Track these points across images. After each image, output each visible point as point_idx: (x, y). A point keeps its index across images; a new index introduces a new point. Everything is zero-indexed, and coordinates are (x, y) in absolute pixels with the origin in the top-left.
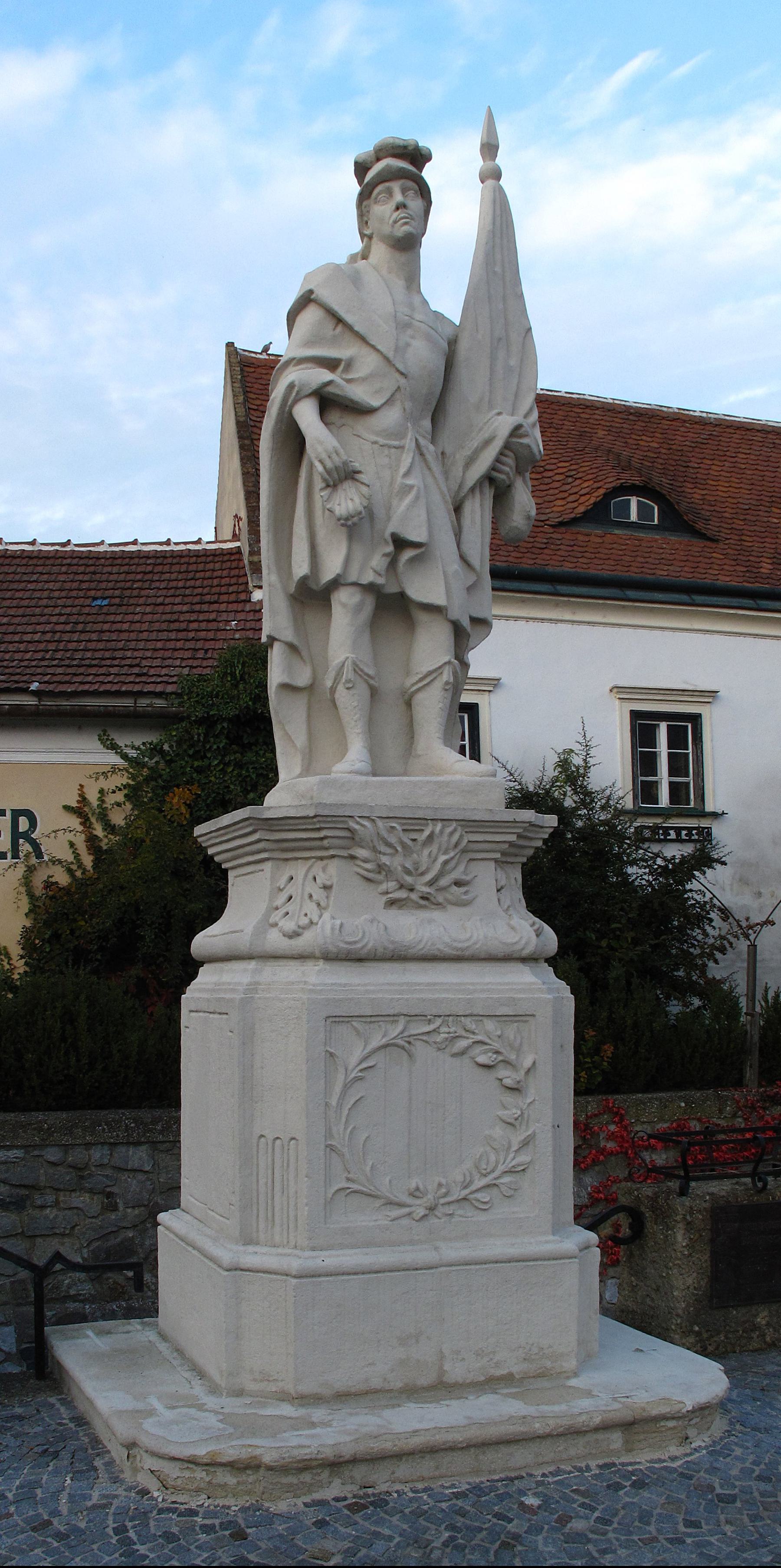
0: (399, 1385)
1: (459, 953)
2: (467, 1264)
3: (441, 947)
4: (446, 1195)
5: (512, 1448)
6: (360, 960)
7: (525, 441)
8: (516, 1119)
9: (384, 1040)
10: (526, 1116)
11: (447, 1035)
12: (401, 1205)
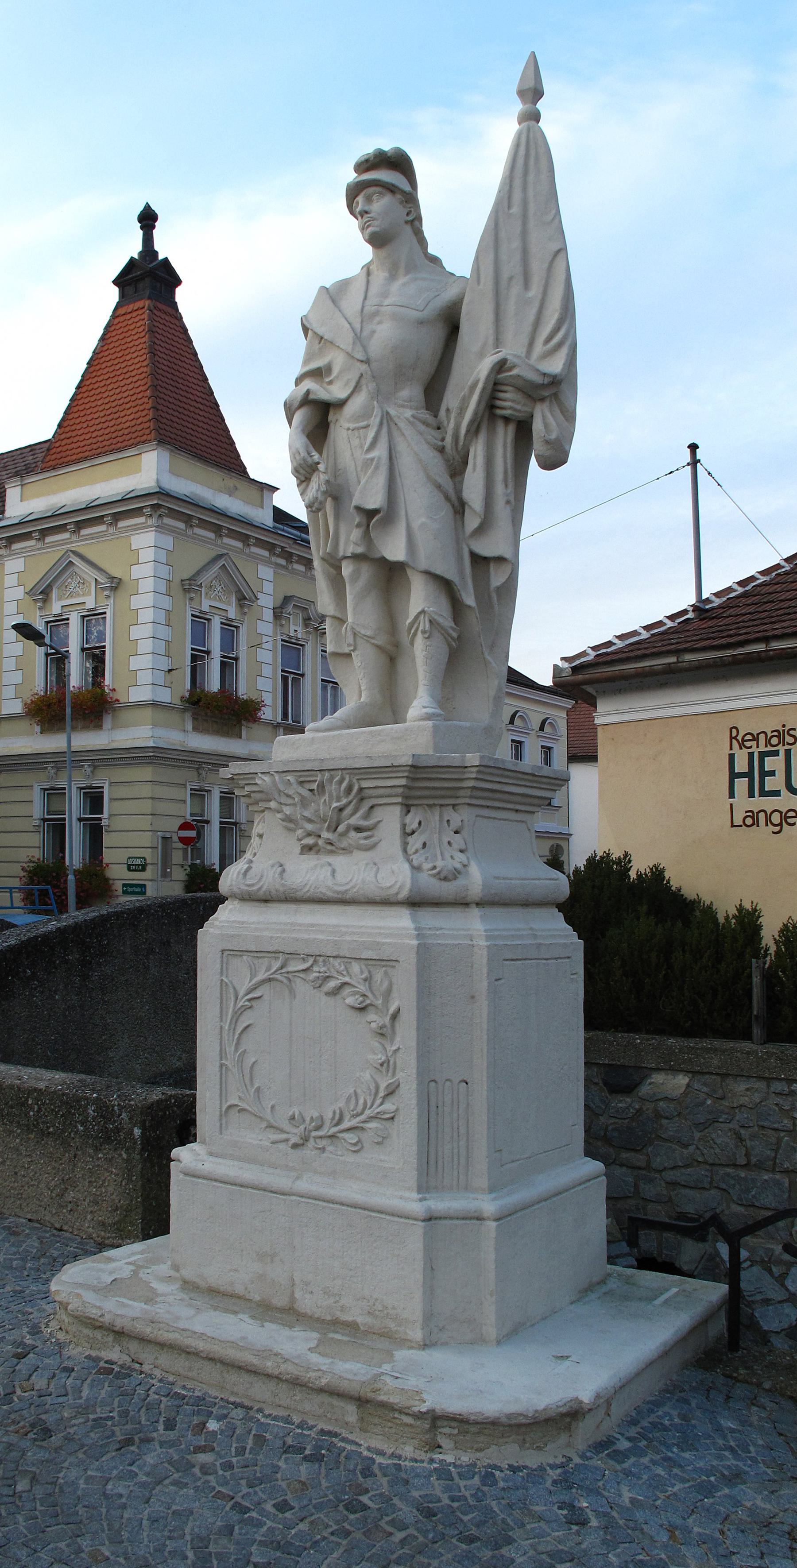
0: (257, 1298)
1: (340, 896)
2: (316, 1199)
3: (324, 891)
4: (318, 1128)
5: (253, 1378)
6: (266, 901)
7: (515, 372)
8: (382, 1065)
9: (266, 974)
10: (391, 1062)
11: (317, 974)
12: (282, 1131)
